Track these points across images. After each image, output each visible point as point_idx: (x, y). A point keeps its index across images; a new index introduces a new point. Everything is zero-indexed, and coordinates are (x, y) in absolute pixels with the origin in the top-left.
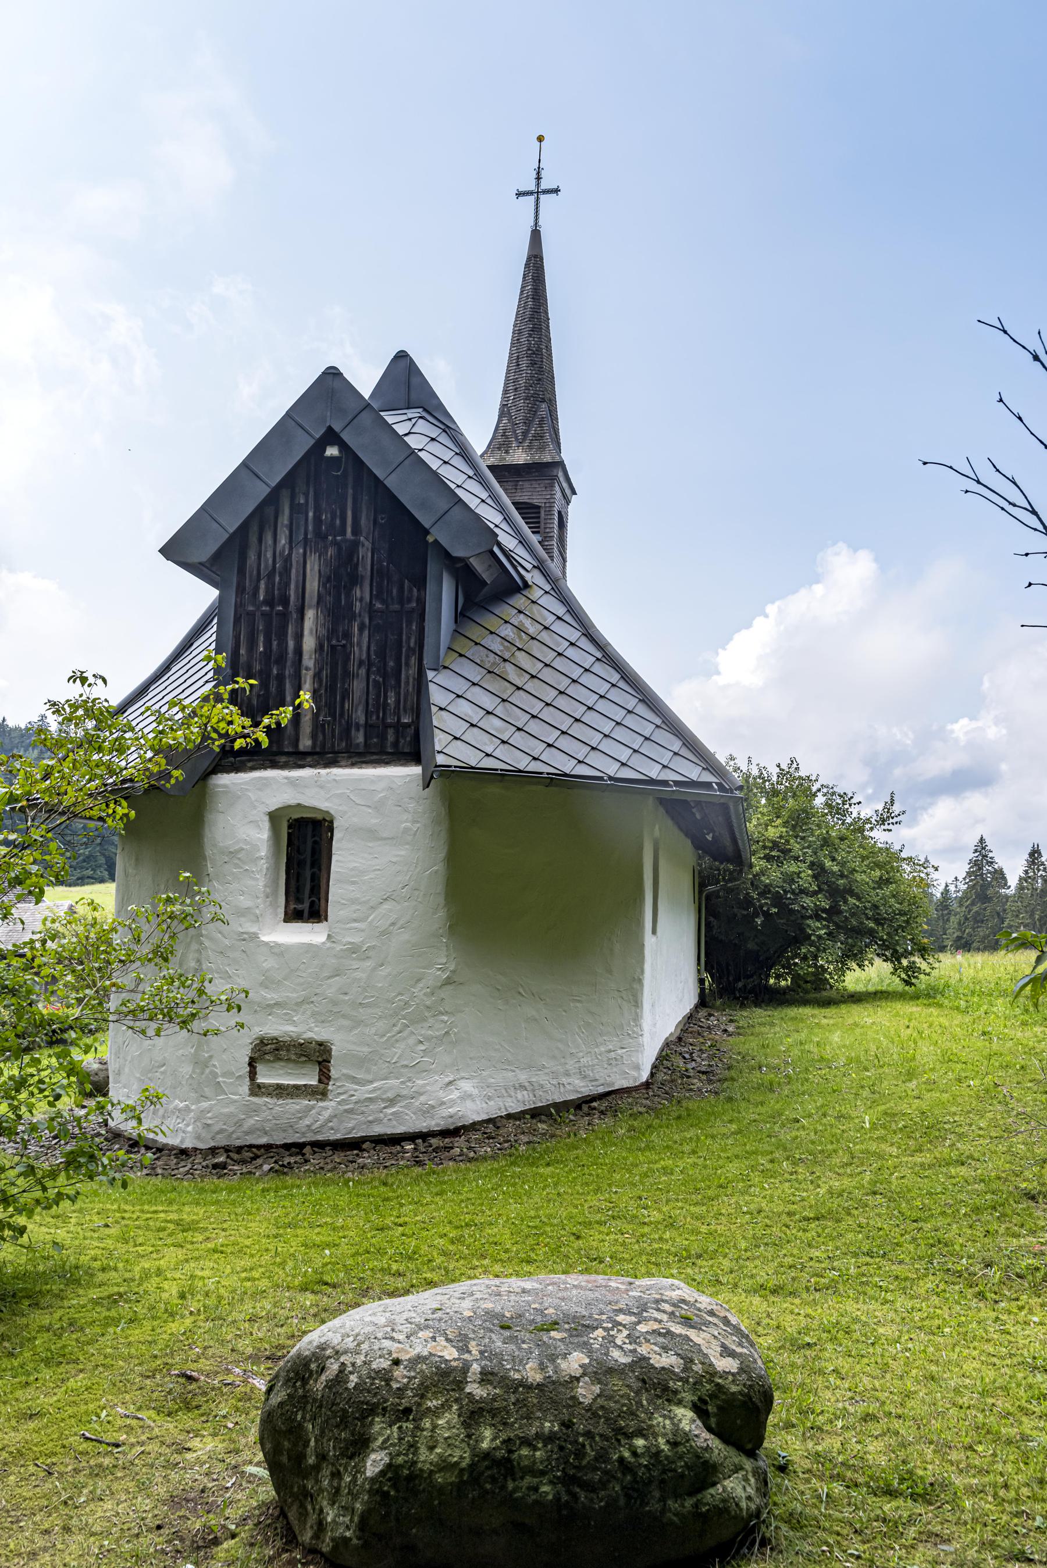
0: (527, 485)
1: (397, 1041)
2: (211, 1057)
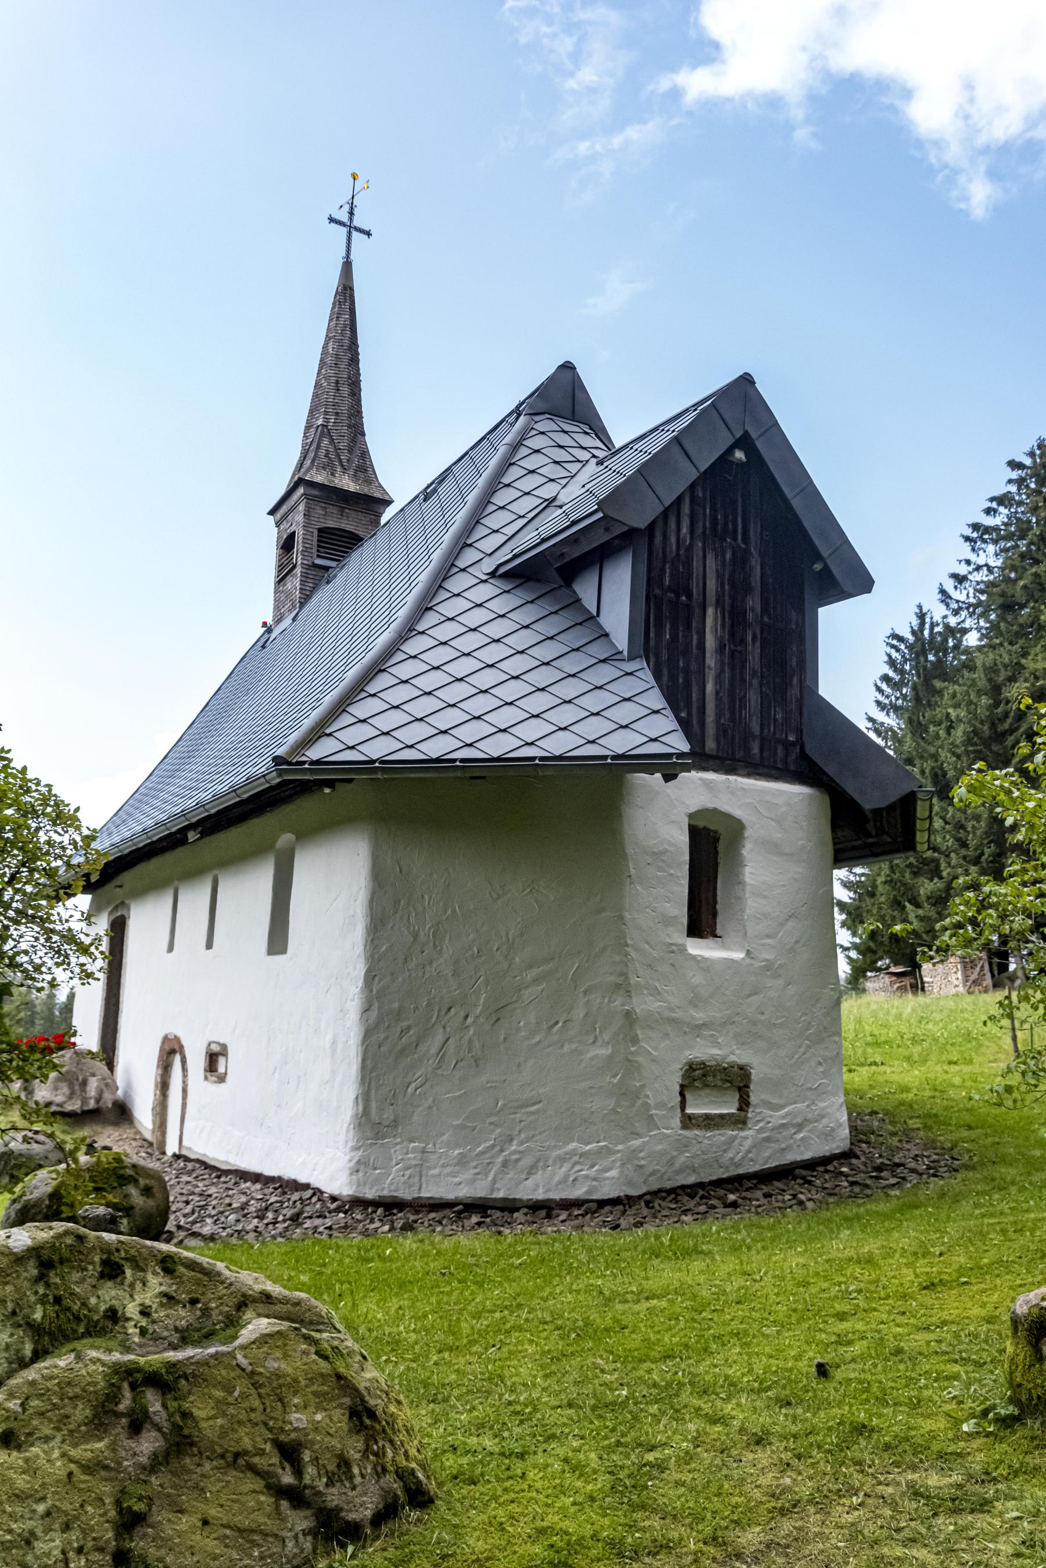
0: (352, 514)
1: (803, 1063)
2: (643, 1086)
